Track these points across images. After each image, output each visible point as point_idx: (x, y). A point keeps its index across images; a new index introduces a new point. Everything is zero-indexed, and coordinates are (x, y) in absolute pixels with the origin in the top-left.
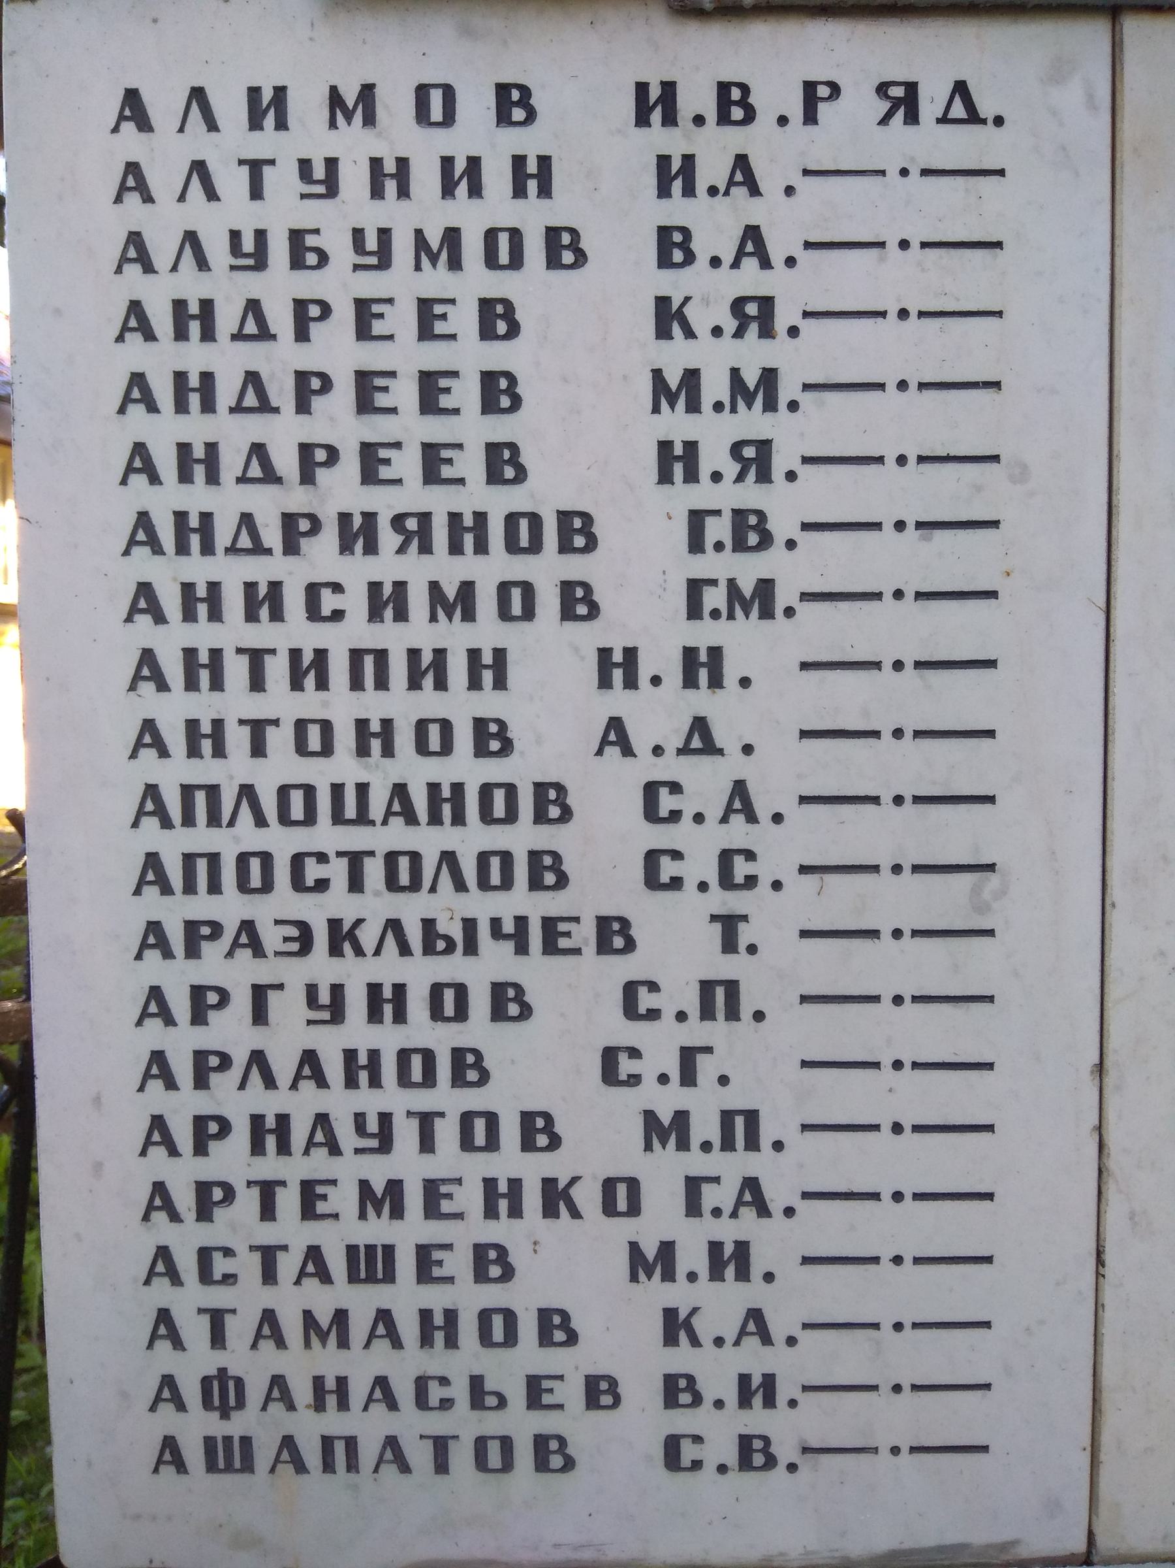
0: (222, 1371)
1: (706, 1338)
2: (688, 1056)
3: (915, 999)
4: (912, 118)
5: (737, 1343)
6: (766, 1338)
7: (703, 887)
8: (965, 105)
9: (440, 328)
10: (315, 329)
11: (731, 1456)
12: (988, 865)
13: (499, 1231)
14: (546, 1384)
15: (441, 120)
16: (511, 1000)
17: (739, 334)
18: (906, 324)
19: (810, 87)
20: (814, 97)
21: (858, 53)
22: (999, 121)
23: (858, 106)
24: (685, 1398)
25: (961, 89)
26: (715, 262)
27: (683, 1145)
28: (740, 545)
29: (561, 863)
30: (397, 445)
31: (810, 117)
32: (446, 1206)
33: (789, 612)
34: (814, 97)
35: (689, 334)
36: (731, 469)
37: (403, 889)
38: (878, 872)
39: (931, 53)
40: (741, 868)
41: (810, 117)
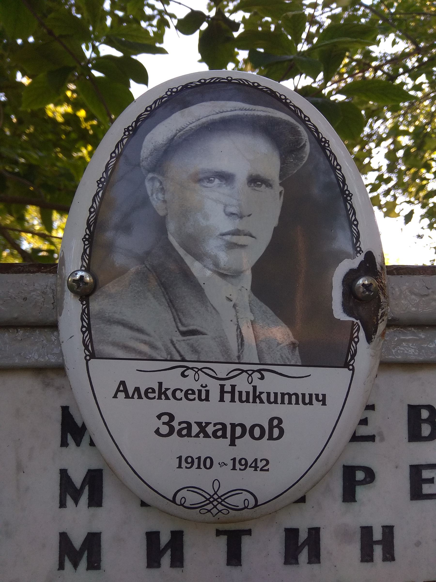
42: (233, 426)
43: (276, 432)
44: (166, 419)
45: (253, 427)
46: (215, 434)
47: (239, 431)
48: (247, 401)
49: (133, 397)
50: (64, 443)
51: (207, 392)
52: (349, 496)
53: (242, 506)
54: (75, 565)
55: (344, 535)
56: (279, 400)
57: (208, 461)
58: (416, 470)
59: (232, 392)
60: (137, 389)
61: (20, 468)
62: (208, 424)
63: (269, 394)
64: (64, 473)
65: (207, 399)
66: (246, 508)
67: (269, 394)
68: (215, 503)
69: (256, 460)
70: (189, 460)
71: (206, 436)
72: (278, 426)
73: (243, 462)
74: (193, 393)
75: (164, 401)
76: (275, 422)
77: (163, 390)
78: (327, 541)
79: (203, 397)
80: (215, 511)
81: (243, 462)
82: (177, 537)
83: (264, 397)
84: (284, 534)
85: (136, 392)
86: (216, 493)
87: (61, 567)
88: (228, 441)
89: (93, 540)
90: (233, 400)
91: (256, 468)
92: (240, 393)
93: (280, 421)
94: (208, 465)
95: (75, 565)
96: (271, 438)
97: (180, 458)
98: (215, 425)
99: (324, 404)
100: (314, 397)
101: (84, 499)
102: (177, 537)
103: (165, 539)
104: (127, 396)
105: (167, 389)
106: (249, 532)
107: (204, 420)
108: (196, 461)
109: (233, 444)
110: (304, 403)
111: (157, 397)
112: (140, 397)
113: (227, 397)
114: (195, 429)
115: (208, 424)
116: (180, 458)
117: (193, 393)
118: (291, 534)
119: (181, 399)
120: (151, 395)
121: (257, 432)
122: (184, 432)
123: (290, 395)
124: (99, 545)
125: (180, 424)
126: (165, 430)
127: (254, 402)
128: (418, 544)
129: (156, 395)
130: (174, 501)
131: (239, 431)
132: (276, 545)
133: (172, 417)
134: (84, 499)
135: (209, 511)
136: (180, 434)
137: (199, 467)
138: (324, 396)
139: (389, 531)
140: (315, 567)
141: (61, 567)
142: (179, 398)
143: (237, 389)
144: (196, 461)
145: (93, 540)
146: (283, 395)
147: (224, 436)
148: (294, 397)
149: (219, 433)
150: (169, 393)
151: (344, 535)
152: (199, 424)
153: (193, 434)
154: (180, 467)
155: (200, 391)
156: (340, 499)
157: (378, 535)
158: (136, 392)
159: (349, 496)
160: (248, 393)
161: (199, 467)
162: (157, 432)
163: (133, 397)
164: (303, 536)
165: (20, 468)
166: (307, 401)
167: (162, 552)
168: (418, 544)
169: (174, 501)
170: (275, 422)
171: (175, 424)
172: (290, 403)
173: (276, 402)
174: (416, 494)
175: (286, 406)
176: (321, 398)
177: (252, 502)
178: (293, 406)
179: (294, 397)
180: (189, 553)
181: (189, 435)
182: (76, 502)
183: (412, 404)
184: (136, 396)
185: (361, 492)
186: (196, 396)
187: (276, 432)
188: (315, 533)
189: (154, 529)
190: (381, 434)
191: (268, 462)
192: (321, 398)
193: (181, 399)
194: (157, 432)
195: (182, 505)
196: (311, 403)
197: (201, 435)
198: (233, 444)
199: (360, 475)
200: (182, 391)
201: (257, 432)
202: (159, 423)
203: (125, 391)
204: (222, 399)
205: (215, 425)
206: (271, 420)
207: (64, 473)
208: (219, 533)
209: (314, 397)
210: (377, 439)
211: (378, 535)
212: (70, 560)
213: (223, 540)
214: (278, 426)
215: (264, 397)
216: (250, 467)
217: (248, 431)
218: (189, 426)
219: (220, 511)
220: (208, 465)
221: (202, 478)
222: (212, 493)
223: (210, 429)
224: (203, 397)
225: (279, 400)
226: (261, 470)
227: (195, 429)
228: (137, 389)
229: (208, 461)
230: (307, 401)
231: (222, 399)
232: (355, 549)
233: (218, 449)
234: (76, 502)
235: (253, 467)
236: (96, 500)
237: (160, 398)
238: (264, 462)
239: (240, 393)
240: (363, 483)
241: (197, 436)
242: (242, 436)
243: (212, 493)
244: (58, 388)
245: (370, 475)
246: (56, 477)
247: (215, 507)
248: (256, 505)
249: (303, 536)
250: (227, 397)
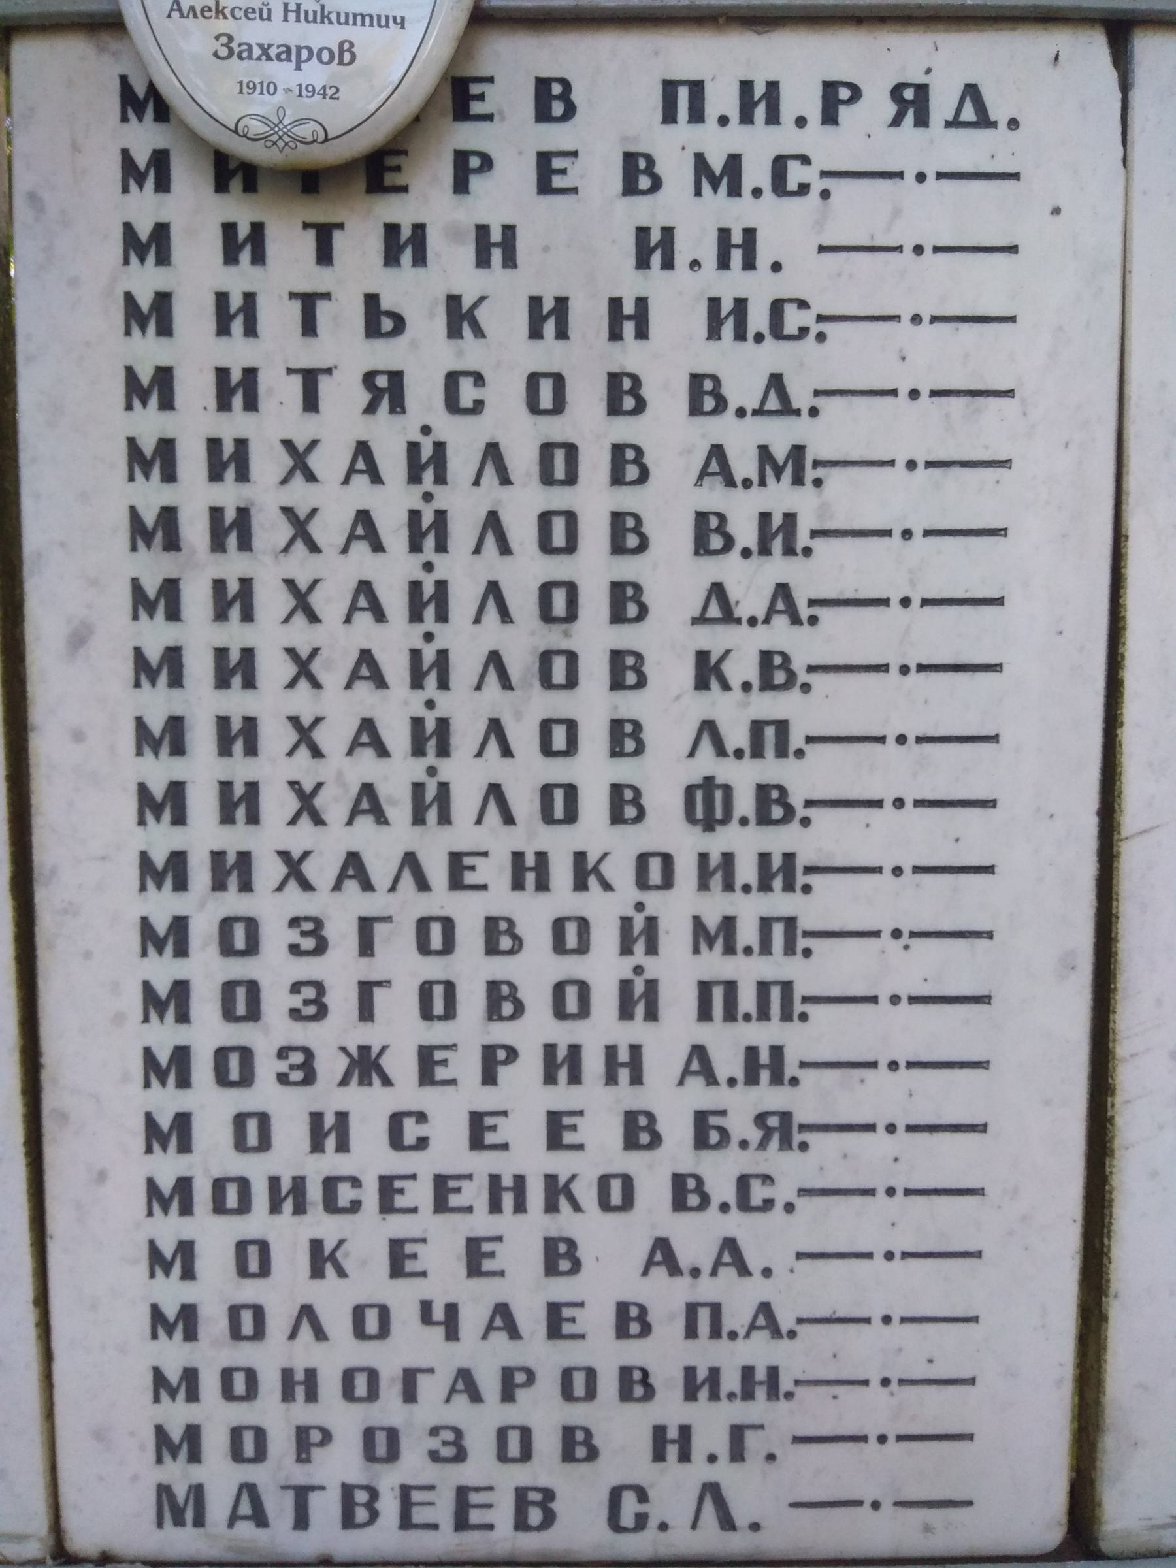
0: (709, 781)
1: (735, 681)
2: (737, 1433)
3: (940, 176)
4: (922, 121)
5: (748, 1335)
6: (776, 1333)
7: (723, 121)
8: (975, 109)
9: (557, 182)
10: (475, 182)
11: (752, 674)
12: (996, 665)
13: (578, 1414)
14: (566, 1121)
15: (564, 682)
16: (629, 530)
17: (763, 1145)
18: (886, 1330)
19: (830, 88)
20: (835, 99)
21: (878, 60)
22: (1013, 124)
23: (877, 105)
24: (564, 1265)
25: (972, 91)
26: (746, 687)
27: (735, 191)
28: (764, 819)
29: (642, 664)
30: (413, 1177)
31: (830, 117)
32: (441, 1073)
33: (800, 753)
34: (835, 99)
35: (726, 687)
36: (755, 1135)
37: (558, 551)
38: (888, 605)
39: (948, 61)
40: (758, 1193)
41: (830, 117)
42: (299, 49)
43: (347, 57)
44: (224, 40)
45: (321, 51)
46: (278, 56)
47: (305, 54)
48: (315, 21)
49: (188, 17)
50: (124, 119)
51: (269, 10)
52: (461, 186)
53: (310, 139)
54: (142, 260)
55: (453, 233)
56: (351, 22)
57: (272, 86)
58: (544, 158)
59: (298, 11)
60: (192, 8)
61: (75, 148)
62: (270, 46)
63: (339, 14)
64: (125, 154)
65: (269, 18)
66: (315, 141)
67: (339, 14)
68: (281, 133)
69: (324, 87)
70: (251, 85)
71: (269, 58)
72: (349, 50)
73: (310, 88)
74: (254, 11)
75: (221, 20)
76: (346, 46)
78: (434, 241)
79: (265, 16)
80: (281, 144)
81: (310, 88)
82: (257, 229)
83: (333, 17)
84: (382, 230)
86: (281, 122)
87: (126, 262)
88: (293, 65)
89: (161, 232)
90: (298, 20)
91: (324, 95)
92: (307, 13)
93: (352, 45)
94: (272, 91)
95: (142, 260)
96: (341, 63)
97: (241, 83)
98: (278, 47)
99: (403, 27)
101: (150, 183)
102: (257, 229)
103: (243, 231)
104: (182, 16)
105: (224, 8)
106: (341, 226)
107: (266, 42)
108: (258, 87)
109: (298, 68)
110: (380, 26)
112: (195, 16)
113: (292, 16)
114: (257, 52)
115: (270, 46)
116: (241, 83)
117: (254, 11)
118: (392, 230)
120: (207, 14)
121: (325, 56)
122: (245, 55)
123: (363, 16)
124: (168, 237)
125: (240, 45)
126: (224, 52)
127: (322, 22)
128: (546, 249)
129: (213, 14)
130: (236, 132)
131: (305, 54)
132: (375, 244)
133: (231, 38)
134: (150, 183)
135: (275, 143)
136: (240, 57)
137: (262, 93)
138: (403, 19)
139: (509, 231)
140: (421, 271)
141: (126, 262)
143: (303, 8)
144: (258, 87)
145: (161, 232)
146: (355, 16)
147: (289, 59)
149: (283, 56)
150: (227, 12)
151: (453, 233)
152: (261, 46)
153: (255, 55)
154: (241, 92)
155: (261, 11)
156: (451, 190)
157: (496, 236)
159: (461, 186)
160: (315, 13)
161: (262, 93)
162: (216, 55)
163: (188, 17)
164: (406, 233)
165: (75, 148)
167: (241, 247)
168: (546, 249)
169: (236, 132)
170: (346, 46)
171: (234, 45)
172: (363, 24)
173: (347, 23)
174: (545, 187)
175: (359, 28)
176: (399, 20)
177: (321, 137)
178: (367, 28)
180: (272, 248)
181: (250, 57)
182: (141, 187)
183: (541, 75)
184: (191, 15)
185: (476, 182)
186: (257, 15)
187: (347, 57)
188: (419, 230)
189: (231, 220)
190: (501, 113)
191: (338, 90)
192: (399, 20)
194: (216, 55)
195: (245, 136)
196: (387, 26)
197: (264, 58)
198: (298, 68)
199: (475, 162)
201: (325, 56)
202: (216, 45)
203: (180, 10)
204: (286, 19)
205: (278, 47)
206: (341, 44)
207: (125, 154)
208: (306, 226)
210: (496, 118)
211: (496, 236)
212: (137, 254)
213: (311, 235)
214: (349, 50)
215: (333, 17)
217: (315, 54)
218: (250, 47)
219: (286, 144)
220: (272, 91)
221: (263, 105)
222: (277, 122)
223: (273, 52)
224: (265, 16)
225: (351, 22)
226: (331, 98)
227: (257, 52)
228: (192, 8)
229: (272, 86)
231: (286, 19)
232: (468, 252)
233: (283, 73)
234: (141, 187)
236: (163, 185)
237: (217, 17)
238: (334, 90)
239: (307, 13)
240: (480, 170)
241: (259, 59)
242: (309, 59)
243: (277, 122)
244: (114, 54)
245: (487, 162)
246: (118, 158)
247: (280, 138)
248: (326, 140)
249: (406, 233)
250: (292, 16)
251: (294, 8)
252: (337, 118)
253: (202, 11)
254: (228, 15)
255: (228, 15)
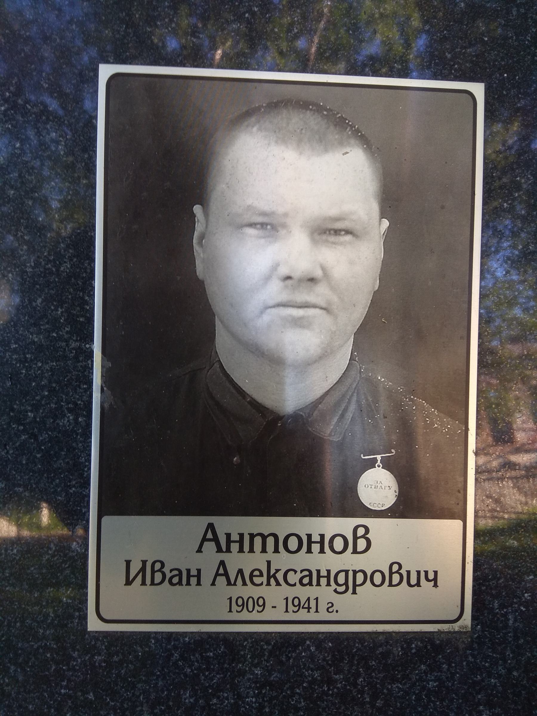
43: (362, 544)
77: (272, 572)
85: (131, 580)
100: (423, 575)
104: (229, 583)
105: (277, 571)
111: (265, 583)
119: (295, 585)
120: (257, 580)
121: (378, 578)
123: (264, 538)
129: (264, 579)
142: (292, 582)
148: (270, 541)
158: (131, 580)
163: (235, 584)
166: (413, 581)
176: (431, 576)
179: (270, 541)
184: (240, 581)
187: (362, 544)
192: (431, 576)
193: (295, 585)
196: (418, 584)
200: (295, 572)
201: (378, 578)
203: (226, 574)
209: (423, 575)
216: (303, 608)
230: (413, 581)
235: (306, 608)
251: (318, 539)
252: (307, 401)
253: (251, 576)
254: (281, 581)
255: (281, 581)
